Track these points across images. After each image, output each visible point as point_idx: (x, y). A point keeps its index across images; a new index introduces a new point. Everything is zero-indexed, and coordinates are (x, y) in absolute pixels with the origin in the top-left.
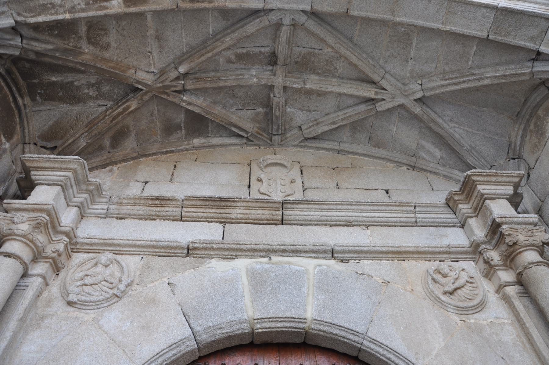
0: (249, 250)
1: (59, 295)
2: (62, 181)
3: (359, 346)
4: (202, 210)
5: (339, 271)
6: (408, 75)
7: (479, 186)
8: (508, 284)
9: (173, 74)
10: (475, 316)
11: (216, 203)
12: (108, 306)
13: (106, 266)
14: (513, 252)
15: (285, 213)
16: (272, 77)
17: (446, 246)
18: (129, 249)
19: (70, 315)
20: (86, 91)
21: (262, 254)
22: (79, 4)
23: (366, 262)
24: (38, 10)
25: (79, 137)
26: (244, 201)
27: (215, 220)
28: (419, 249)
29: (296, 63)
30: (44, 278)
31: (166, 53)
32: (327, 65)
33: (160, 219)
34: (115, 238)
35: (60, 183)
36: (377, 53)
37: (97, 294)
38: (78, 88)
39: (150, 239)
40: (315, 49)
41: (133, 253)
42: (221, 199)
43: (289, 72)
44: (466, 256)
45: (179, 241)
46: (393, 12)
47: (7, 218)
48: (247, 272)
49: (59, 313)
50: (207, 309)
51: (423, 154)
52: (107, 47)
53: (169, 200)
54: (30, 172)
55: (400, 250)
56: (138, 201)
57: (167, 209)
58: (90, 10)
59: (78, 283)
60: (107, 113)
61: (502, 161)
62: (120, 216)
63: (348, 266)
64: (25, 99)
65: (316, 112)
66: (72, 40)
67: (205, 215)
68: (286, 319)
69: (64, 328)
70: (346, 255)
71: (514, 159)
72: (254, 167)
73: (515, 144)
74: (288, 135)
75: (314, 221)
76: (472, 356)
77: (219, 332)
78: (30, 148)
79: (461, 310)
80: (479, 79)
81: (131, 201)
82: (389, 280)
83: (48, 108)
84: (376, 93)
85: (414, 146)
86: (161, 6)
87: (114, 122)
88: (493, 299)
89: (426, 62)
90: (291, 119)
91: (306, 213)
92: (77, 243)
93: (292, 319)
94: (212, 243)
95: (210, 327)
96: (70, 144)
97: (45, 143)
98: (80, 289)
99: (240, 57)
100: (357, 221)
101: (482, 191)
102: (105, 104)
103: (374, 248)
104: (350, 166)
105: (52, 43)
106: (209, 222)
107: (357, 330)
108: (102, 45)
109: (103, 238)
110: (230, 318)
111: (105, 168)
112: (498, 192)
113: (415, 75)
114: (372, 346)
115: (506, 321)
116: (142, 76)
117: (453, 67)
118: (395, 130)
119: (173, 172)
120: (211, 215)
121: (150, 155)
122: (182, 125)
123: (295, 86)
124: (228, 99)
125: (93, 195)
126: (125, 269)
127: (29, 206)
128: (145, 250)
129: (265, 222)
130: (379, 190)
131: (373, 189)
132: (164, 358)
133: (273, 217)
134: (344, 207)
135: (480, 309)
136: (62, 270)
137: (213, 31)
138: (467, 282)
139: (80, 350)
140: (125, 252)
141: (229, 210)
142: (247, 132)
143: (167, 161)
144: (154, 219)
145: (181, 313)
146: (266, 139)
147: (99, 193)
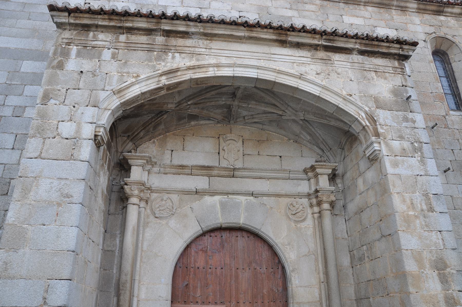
0: (220, 193)
1: (151, 213)
5: (254, 202)
9: (185, 104)
10: (301, 224)
11: (206, 168)
14: (320, 203)
15: (235, 173)
21: (225, 194)
23: (265, 198)
28: (287, 194)
33: (182, 175)
37: (166, 214)
42: (208, 167)
46: (293, 93)
48: (219, 202)
51: (302, 136)
56: (172, 167)
57: (185, 170)
61: (336, 148)
67: (201, 173)
69: (157, 227)
70: (258, 195)
71: (340, 148)
73: (342, 143)
74: (238, 120)
76: (295, 239)
79: (296, 222)
81: (170, 167)
84: (282, 113)
85: (298, 132)
88: (310, 216)
91: (243, 173)
93: (235, 223)
96: (136, 136)
101: (318, 172)
104: (266, 140)
110: (214, 222)
114: (262, 234)
115: (311, 226)
116: (170, 106)
119: (184, 143)
120: (204, 173)
122: (186, 117)
123: (243, 105)
126: (174, 202)
132: (192, 237)
133: (229, 175)
134: (259, 171)
138: (301, 210)
141: (211, 171)
144: (180, 174)
146: (227, 122)
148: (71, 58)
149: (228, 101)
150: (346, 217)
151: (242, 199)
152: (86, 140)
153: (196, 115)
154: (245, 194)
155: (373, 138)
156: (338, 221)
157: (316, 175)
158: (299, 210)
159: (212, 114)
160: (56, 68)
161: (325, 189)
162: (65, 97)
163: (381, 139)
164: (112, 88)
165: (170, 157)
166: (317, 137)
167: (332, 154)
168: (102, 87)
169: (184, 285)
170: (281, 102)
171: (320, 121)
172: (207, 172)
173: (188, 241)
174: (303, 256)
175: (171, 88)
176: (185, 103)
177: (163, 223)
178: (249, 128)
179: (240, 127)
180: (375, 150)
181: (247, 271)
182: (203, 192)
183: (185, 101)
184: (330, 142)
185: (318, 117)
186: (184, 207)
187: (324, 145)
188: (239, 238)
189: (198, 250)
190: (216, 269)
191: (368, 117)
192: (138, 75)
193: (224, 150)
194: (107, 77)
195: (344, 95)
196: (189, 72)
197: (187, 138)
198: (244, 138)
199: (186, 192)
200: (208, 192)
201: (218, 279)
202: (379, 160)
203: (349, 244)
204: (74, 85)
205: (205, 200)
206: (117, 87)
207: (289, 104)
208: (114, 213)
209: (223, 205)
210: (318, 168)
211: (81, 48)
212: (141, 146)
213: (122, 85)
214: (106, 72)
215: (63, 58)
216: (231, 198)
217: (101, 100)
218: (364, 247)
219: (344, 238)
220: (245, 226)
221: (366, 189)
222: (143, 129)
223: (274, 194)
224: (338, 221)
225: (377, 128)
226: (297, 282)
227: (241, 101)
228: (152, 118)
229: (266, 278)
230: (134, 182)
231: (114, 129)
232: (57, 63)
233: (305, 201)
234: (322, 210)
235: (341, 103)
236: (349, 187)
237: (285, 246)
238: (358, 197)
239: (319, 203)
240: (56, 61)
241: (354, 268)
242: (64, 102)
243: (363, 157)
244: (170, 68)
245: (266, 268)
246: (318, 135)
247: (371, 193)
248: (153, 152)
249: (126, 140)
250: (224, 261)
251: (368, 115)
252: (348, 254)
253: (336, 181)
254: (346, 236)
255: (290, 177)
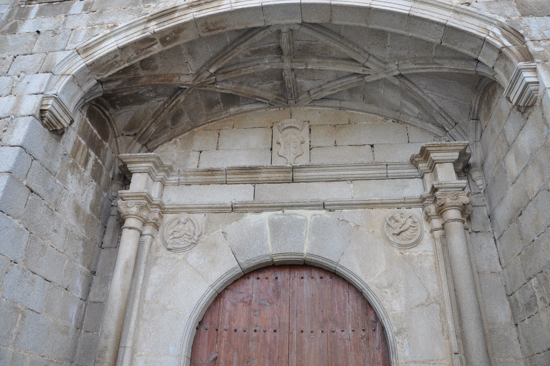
2: (147, 170)
3: (334, 269)
4: (239, 176)
5: (327, 219)
6: (388, 57)
7: (432, 153)
8: (437, 230)
9: (207, 74)
10: (411, 250)
11: (248, 171)
12: (190, 249)
13: (185, 224)
14: (442, 209)
16: (281, 63)
17: (402, 198)
18: (197, 210)
19: (170, 256)
20: (148, 95)
21: (278, 209)
22: (132, 55)
23: (346, 211)
24: (108, 68)
25: (150, 126)
26: (266, 168)
27: (248, 182)
28: (383, 201)
29: (299, 50)
30: (152, 235)
31: (198, 60)
32: (323, 50)
33: (213, 184)
34: (187, 204)
35: (146, 171)
36: (361, 42)
37: (183, 243)
38: (142, 94)
39: (208, 203)
40: (311, 41)
41: (199, 212)
43: (294, 58)
44: (417, 205)
45: (226, 203)
47: (123, 204)
48: (269, 222)
49: (164, 255)
50: (246, 249)
51: (406, 110)
52: (156, 67)
53: (217, 170)
54: (126, 165)
55: (370, 203)
57: (216, 177)
58: (140, 56)
59: (171, 237)
60: (165, 106)
61: (465, 120)
62: (187, 183)
63: (334, 215)
64: (110, 110)
65: (321, 81)
66: (132, 72)
67: (242, 179)
68: (291, 254)
69: (169, 265)
70: (333, 207)
71: (473, 119)
72: (275, 129)
73: (475, 109)
74: (301, 98)
75: (314, 179)
77: (253, 262)
78: (120, 139)
80: (440, 68)
81: (193, 173)
82: (359, 225)
83: (125, 110)
84: (363, 71)
85: (398, 104)
86: (188, 39)
87: (171, 112)
88: (427, 236)
89: (400, 49)
90: (302, 86)
91: (308, 174)
92: (165, 208)
93: (295, 254)
94: (246, 204)
95: (248, 260)
96: (144, 132)
97: (128, 133)
98: (172, 241)
99: (254, 52)
100: (344, 178)
101: (433, 158)
102: (163, 99)
103: (351, 202)
104: (347, 123)
105: (120, 79)
106: (245, 184)
107: (333, 260)
108: (152, 68)
109: (179, 204)
110: (259, 254)
111: (171, 140)
112: (446, 158)
113: (393, 57)
114: (342, 270)
116: (184, 79)
117: (421, 55)
118: (382, 92)
119: (218, 140)
120: (245, 179)
121: (200, 126)
122: (220, 100)
123: (299, 68)
124: (250, 79)
125: (168, 172)
126: (196, 225)
127: (134, 194)
128: (206, 210)
129: (282, 182)
130: (366, 146)
131: (362, 145)
132: (224, 279)
133: (286, 178)
134: (335, 168)
135: (415, 245)
136: (160, 227)
137: (230, 40)
138: (410, 226)
139: (180, 277)
140: (194, 212)
142: (269, 100)
143: (213, 130)
144: (209, 184)
145: (231, 252)
146: (283, 103)
147: (171, 170)
148: (29, 18)
149: (274, 62)
150: (495, 233)
151: (307, 214)
152: (24, 117)
153: (230, 94)
154: (311, 206)
155: (521, 64)
156: (481, 242)
157: (432, 165)
158: (406, 227)
159: (257, 92)
160: (6, 33)
161: (449, 185)
162: (10, 66)
163: (537, 63)
164: (74, 46)
165: (197, 161)
166: (429, 104)
167: (460, 131)
168: (62, 46)
169: (211, 359)
170: (356, 49)
171: (425, 71)
172: (250, 176)
173: (217, 286)
174: (418, 306)
175: (168, 39)
176: (206, 71)
177: (179, 258)
178: (319, 110)
179: (305, 109)
180: (527, 84)
181: (319, 336)
182: (243, 207)
183: (205, 68)
184: (454, 111)
185: (421, 64)
186: (213, 232)
187: (443, 117)
188: (305, 280)
189: (237, 302)
190: (265, 332)
191: (506, 32)
192: (116, 24)
193: (279, 143)
194: (72, 34)
195: (454, 5)
196: (192, 11)
197: (223, 133)
198: (311, 124)
199: (216, 209)
200: (251, 207)
201: (268, 350)
202: (537, 104)
203: (505, 282)
204: (26, 49)
205: (246, 220)
206: (84, 43)
207: (372, 51)
208: (110, 246)
209: (275, 226)
210: (434, 151)
211: (45, 5)
212: (156, 150)
213: (89, 40)
214: (72, 28)
215: (19, 19)
216: (289, 215)
217: (57, 63)
218: (532, 280)
219: (495, 271)
220: (312, 258)
221: (522, 169)
222: (154, 122)
223: (360, 202)
224: (481, 242)
225: (527, 48)
226: (407, 353)
227: (295, 60)
228: (164, 104)
229: (352, 347)
230: (131, 194)
231: (108, 123)
232: (10, 26)
233: (417, 212)
234: (446, 222)
235: (452, 19)
236: (494, 180)
237: (384, 290)
238: (511, 189)
239: (440, 211)
240: (8, 25)
241: (519, 326)
242: (7, 72)
243: (509, 114)
244: (163, 9)
245: (353, 331)
246: (429, 101)
247: (532, 171)
248: (173, 156)
249: (132, 141)
250: (279, 318)
251: (506, 30)
252: (506, 300)
253: (471, 175)
254: (499, 268)
255: (389, 175)
